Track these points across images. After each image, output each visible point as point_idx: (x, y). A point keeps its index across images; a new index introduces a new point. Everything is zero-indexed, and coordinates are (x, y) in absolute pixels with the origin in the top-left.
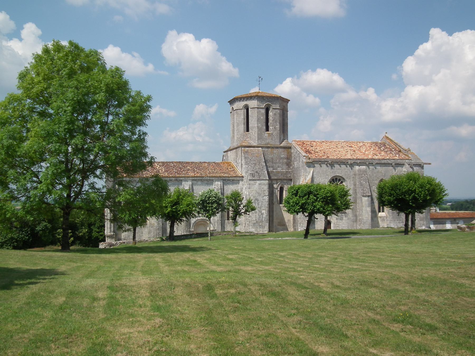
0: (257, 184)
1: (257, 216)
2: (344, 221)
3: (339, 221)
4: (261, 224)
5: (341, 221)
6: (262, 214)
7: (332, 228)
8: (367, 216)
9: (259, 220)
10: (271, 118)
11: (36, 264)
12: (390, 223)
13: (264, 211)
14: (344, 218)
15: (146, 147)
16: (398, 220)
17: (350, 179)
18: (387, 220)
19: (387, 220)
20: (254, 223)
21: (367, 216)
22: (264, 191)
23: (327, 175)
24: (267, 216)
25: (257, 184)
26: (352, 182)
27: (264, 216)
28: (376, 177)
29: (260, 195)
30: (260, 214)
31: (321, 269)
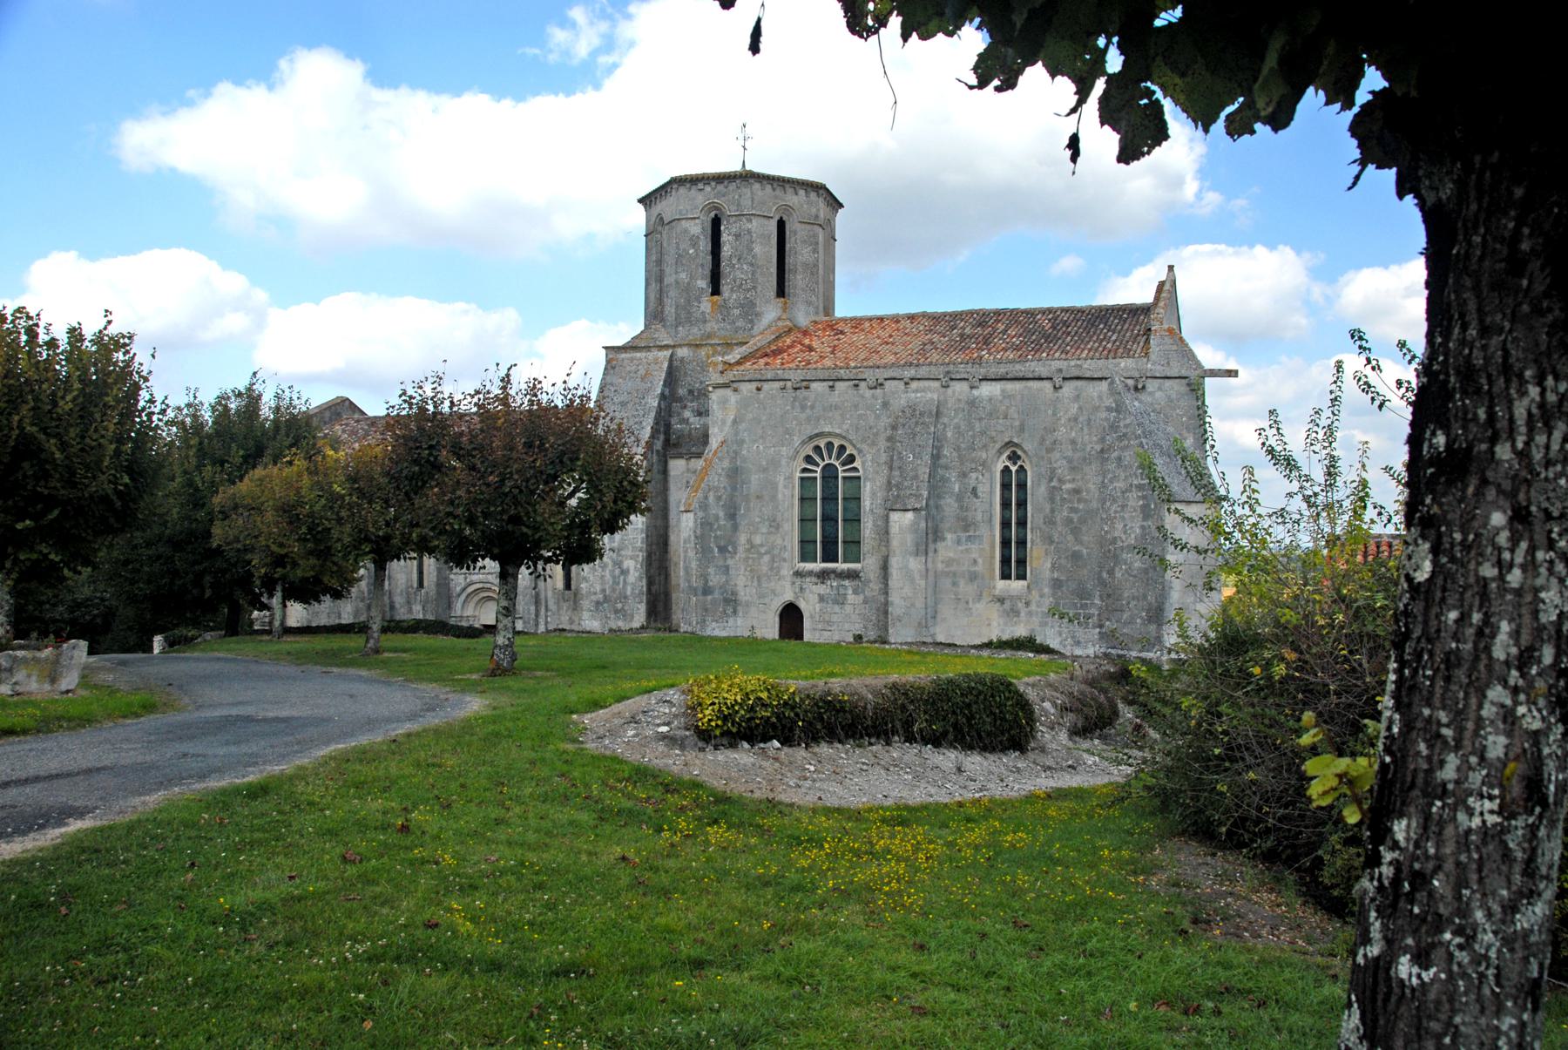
2: (848, 609)
3: (830, 607)
4: (619, 606)
5: (837, 608)
6: (625, 572)
7: (807, 636)
8: (907, 591)
9: (614, 590)
10: (1031, 384)
11: (1078, 643)
13: (629, 564)
14: (851, 597)
15: (75, 334)
17: (874, 444)
18: (1030, 614)
19: (1030, 614)
20: (598, 603)
21: (907, 591)
23: (787, 431)
24: (641, 579)
26: (884, 457)
27: (633, 576)
28: (983, 433)
30: (617, 572)
31: (1488, 649)
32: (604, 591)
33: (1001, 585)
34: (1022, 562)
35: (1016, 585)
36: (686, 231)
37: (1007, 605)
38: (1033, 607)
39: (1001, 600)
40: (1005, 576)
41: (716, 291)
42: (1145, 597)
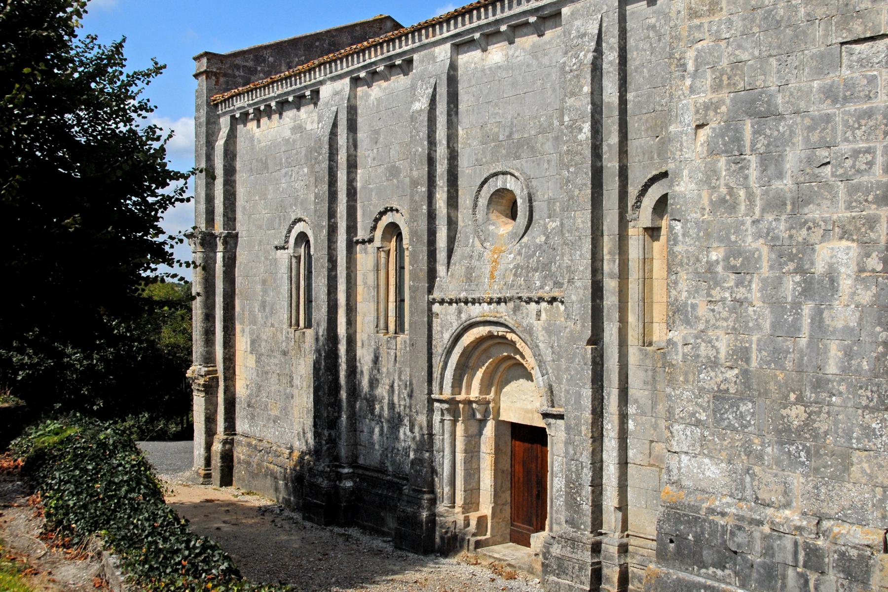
1: (757, 305)
6: (818, 288)
9: (777, 356)
30: (791, 286)
32: (741, 354)
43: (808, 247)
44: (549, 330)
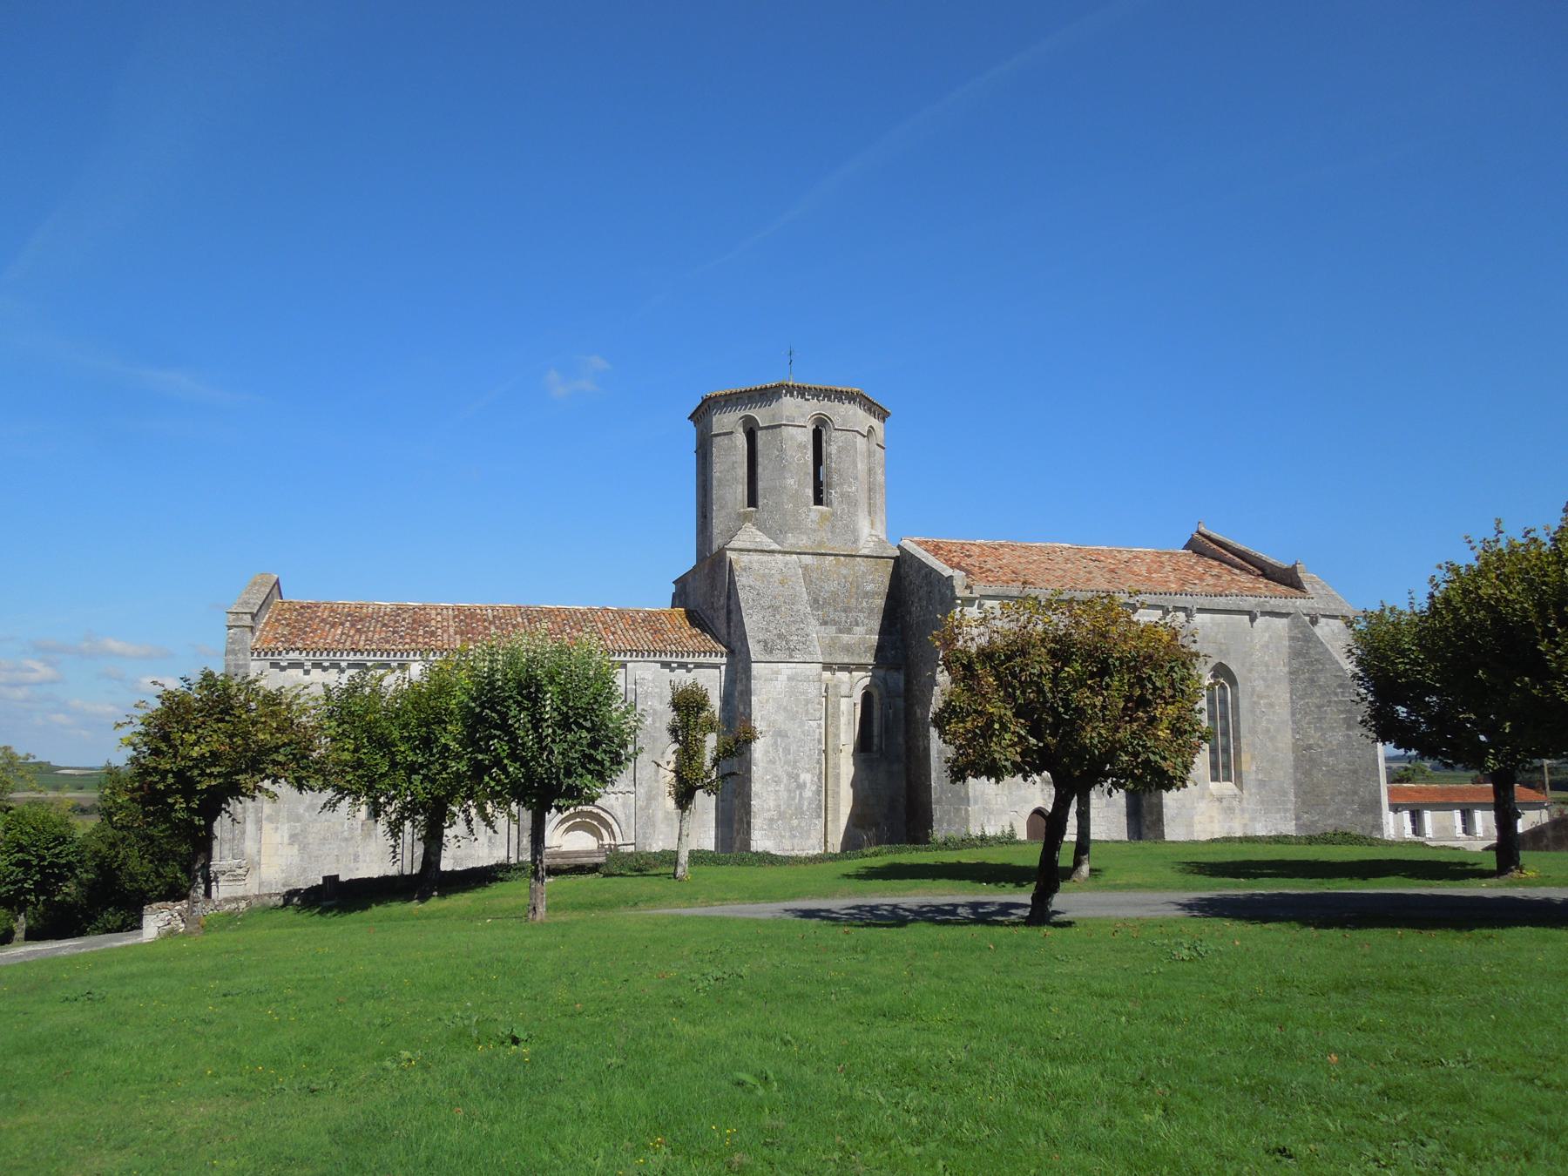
0: (783, 678)
9: (789, 806)
12: (1253, 819)
13: (806, 777)
16: (1278, 811)
18: (1243, 810)
20: (771, 820)
22: (807, 702)
25: (783, 678)
29: (793, 717)
32: (779, 806)
33: (1213, 786)
34: (1227, 767)
35: (1228, 787)
36: (792, 438)
37: (1225, 803)
38: (1245, 804)
39: (1220, 800)
40: (1215, 779)
41: (818, 500)
42: (1355, 793)
43: (798, 775)
44: (624, 805)
